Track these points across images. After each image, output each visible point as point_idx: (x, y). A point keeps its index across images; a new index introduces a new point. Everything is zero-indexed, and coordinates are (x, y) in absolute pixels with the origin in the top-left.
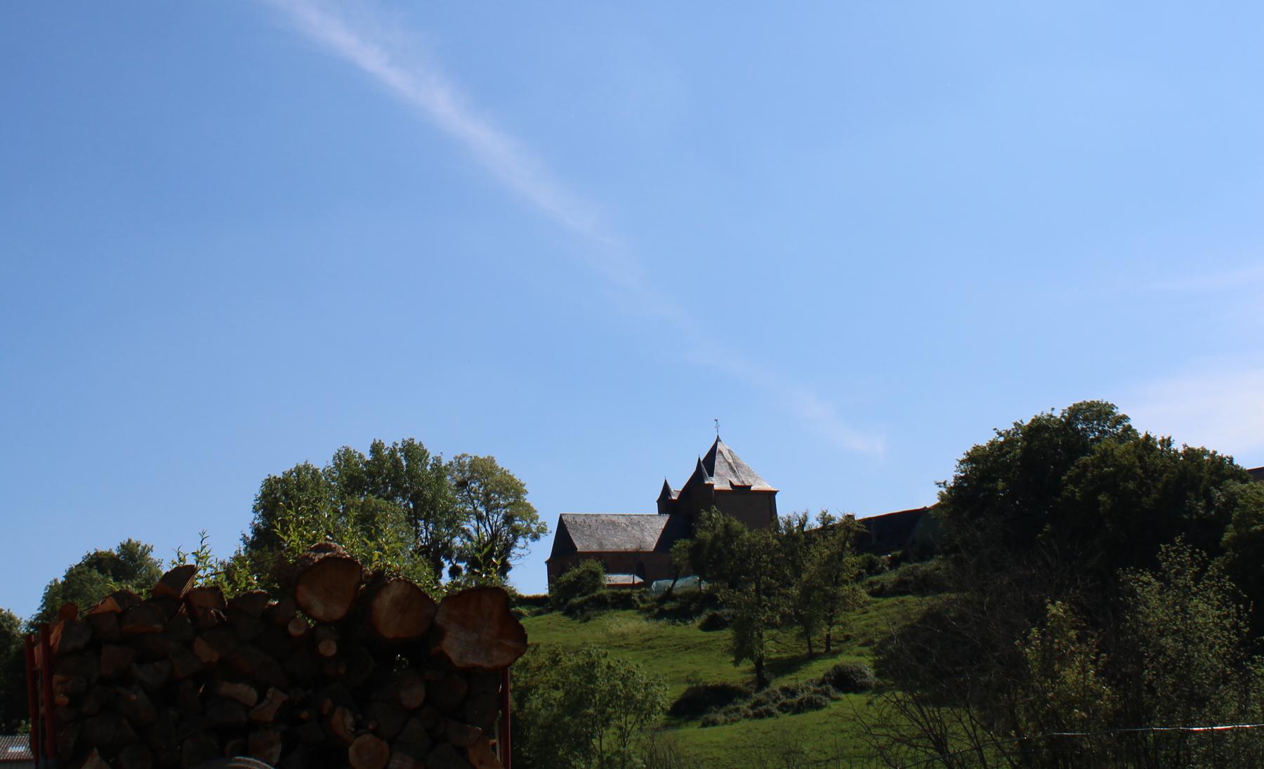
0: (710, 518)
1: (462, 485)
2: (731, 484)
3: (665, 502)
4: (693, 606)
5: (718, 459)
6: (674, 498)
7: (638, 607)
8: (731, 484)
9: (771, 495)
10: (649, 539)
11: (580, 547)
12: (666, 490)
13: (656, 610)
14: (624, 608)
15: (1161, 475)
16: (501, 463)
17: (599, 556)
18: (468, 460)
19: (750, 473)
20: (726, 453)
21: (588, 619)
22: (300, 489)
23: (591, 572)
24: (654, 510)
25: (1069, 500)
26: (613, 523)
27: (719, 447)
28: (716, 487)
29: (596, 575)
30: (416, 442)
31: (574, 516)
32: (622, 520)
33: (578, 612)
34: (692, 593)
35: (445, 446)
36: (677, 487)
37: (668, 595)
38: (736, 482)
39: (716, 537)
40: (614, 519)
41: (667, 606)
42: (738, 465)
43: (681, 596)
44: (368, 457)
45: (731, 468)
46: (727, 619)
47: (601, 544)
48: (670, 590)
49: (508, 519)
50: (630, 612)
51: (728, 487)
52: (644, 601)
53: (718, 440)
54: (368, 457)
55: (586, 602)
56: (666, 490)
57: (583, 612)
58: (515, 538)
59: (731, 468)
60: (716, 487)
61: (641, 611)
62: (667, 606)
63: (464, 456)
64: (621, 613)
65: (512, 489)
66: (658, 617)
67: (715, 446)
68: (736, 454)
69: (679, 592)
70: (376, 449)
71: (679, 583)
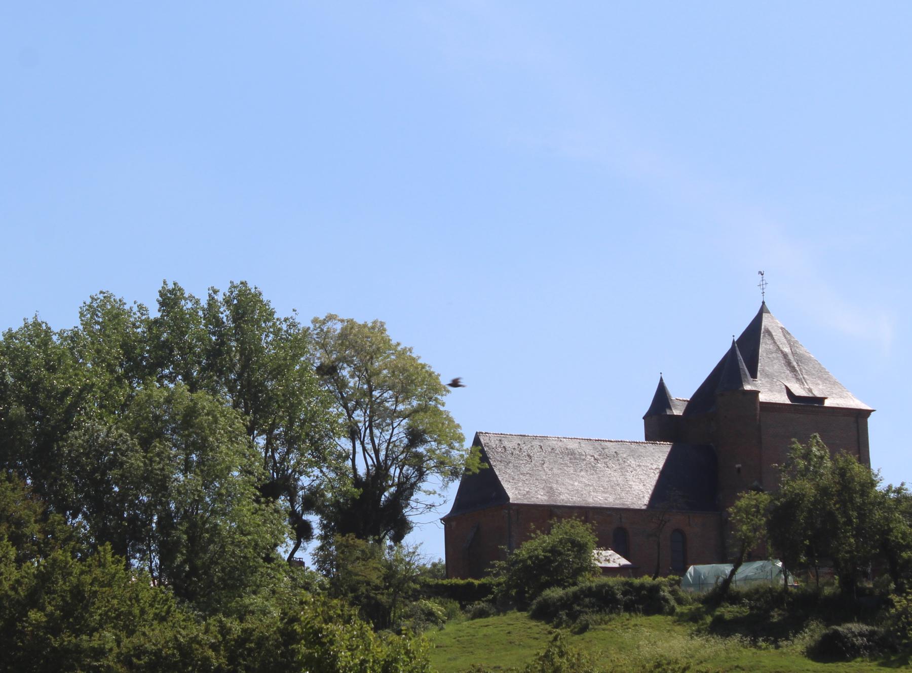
0: (807, 456)
1: (328, 371)
2: (790, 393)
3: (659, 421)
4: (776, 616)
5: (765, 347)
6: (678, 412)
7: (672, 612)
8: (790, 393)
9: (861, 416)
10: (637, 487)
11: (515, 492)
12: (662, 397)
13: (709, 619)
14: (648, 612)
15: (62, 400)
16: (398, 334)
17: (586, 513)
18: (338, 327)
19: (822, 375)
20: (778, 335)
21: (584, 629)
22: (52, 369)
23: (574, 543)
24: (638, 432)
25: (739, 447)
26: (571, 453)
27: (766, 322)
28: (762, 398)
29: (581, 549)
30: (251, 285)
31: (501, 437)
32: (587, 449)
33: (563, 615)
34: (771, 590)
35: (300, 299)
36: (682, 392)
37: (723, 593)
38: (798, 391)
39: (824, 491)
40: (572, 445)
41: (728, 611)
42: (801, 359)
43: (748, 595)
44: (154, 313)
45: (789, 364)
46: (859, 641)
47: (551, 491)
48: (728, 581)
49: (415, 437)
50: (657, 618)
51: (784, 399)
52: (680, 601)
53: (763, 310)
54: (154, 313)
55: (576, 597)
56: (662, 397)
57: (573, 616)
58: (421, 475)
59: (789, 364)
60: (762, 398)
61: (682, 619)
62: (728, 611)
63: (331, 318)
64: (640, 619)
65: (414, 381)
66: (722, 628)
67: (758, 320)
68: (796, 336)
69: (744, 588)
70: (170, 299)
71: (748, 570)
